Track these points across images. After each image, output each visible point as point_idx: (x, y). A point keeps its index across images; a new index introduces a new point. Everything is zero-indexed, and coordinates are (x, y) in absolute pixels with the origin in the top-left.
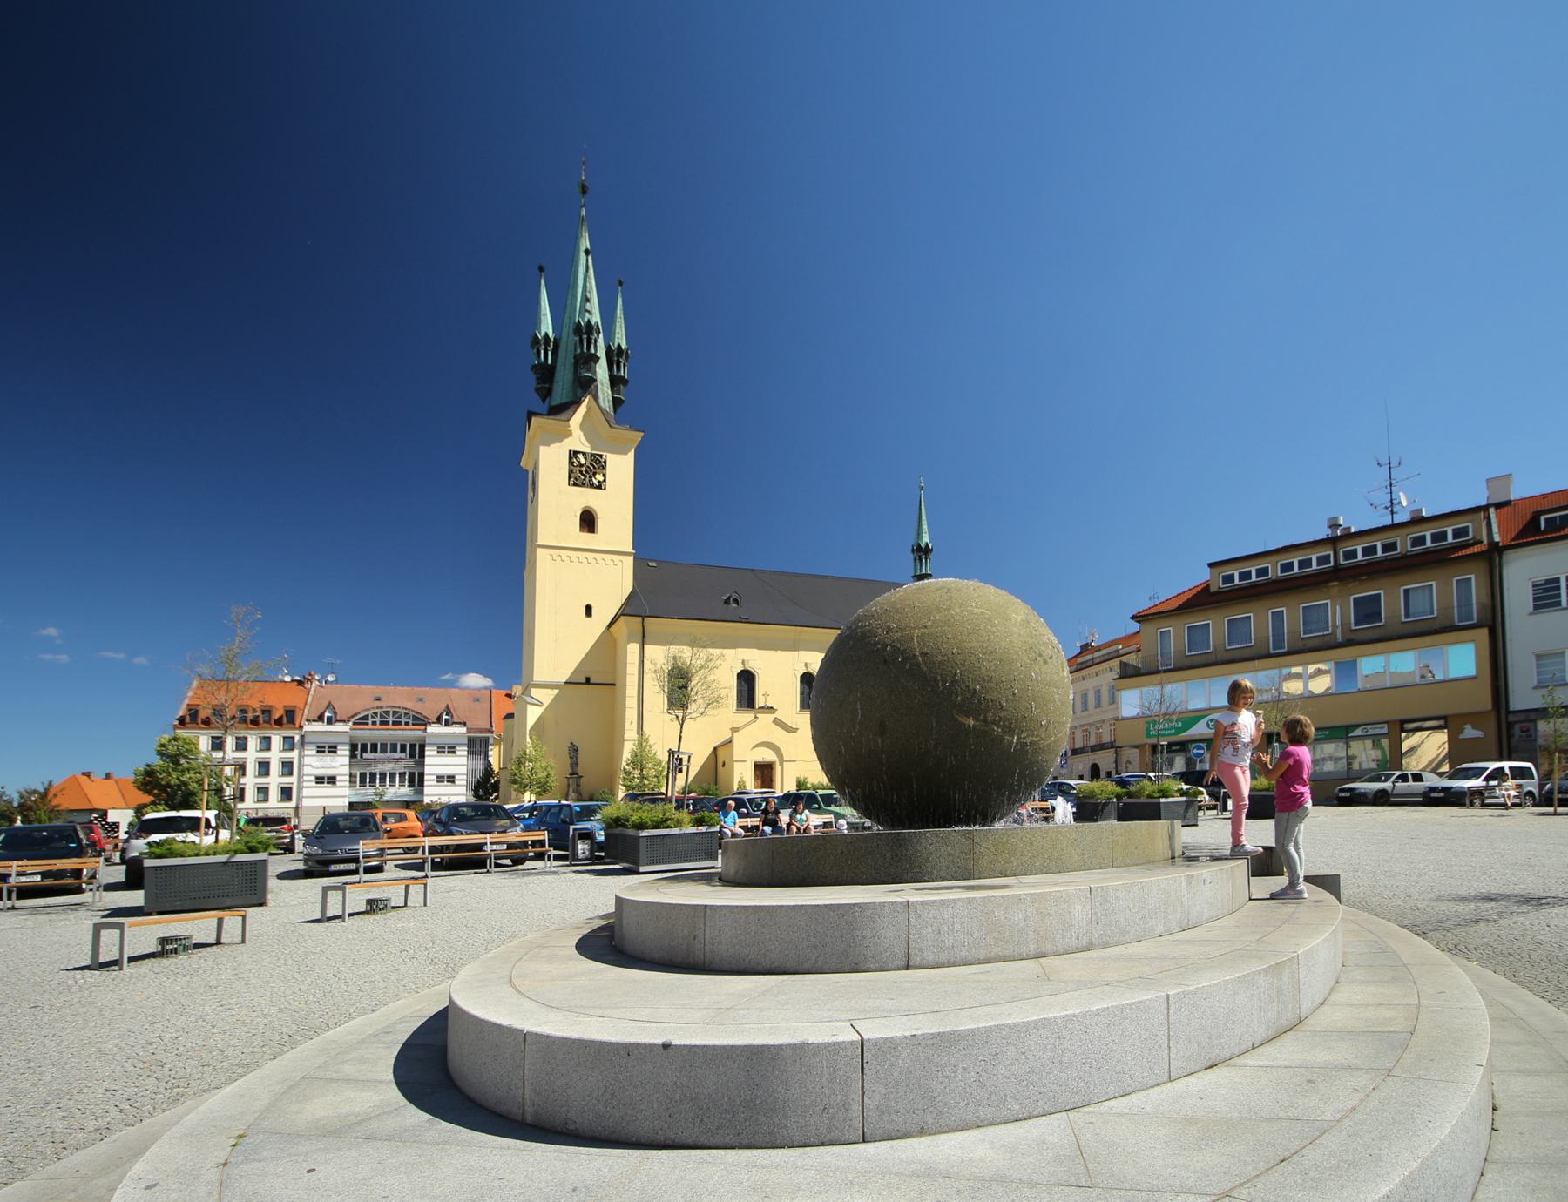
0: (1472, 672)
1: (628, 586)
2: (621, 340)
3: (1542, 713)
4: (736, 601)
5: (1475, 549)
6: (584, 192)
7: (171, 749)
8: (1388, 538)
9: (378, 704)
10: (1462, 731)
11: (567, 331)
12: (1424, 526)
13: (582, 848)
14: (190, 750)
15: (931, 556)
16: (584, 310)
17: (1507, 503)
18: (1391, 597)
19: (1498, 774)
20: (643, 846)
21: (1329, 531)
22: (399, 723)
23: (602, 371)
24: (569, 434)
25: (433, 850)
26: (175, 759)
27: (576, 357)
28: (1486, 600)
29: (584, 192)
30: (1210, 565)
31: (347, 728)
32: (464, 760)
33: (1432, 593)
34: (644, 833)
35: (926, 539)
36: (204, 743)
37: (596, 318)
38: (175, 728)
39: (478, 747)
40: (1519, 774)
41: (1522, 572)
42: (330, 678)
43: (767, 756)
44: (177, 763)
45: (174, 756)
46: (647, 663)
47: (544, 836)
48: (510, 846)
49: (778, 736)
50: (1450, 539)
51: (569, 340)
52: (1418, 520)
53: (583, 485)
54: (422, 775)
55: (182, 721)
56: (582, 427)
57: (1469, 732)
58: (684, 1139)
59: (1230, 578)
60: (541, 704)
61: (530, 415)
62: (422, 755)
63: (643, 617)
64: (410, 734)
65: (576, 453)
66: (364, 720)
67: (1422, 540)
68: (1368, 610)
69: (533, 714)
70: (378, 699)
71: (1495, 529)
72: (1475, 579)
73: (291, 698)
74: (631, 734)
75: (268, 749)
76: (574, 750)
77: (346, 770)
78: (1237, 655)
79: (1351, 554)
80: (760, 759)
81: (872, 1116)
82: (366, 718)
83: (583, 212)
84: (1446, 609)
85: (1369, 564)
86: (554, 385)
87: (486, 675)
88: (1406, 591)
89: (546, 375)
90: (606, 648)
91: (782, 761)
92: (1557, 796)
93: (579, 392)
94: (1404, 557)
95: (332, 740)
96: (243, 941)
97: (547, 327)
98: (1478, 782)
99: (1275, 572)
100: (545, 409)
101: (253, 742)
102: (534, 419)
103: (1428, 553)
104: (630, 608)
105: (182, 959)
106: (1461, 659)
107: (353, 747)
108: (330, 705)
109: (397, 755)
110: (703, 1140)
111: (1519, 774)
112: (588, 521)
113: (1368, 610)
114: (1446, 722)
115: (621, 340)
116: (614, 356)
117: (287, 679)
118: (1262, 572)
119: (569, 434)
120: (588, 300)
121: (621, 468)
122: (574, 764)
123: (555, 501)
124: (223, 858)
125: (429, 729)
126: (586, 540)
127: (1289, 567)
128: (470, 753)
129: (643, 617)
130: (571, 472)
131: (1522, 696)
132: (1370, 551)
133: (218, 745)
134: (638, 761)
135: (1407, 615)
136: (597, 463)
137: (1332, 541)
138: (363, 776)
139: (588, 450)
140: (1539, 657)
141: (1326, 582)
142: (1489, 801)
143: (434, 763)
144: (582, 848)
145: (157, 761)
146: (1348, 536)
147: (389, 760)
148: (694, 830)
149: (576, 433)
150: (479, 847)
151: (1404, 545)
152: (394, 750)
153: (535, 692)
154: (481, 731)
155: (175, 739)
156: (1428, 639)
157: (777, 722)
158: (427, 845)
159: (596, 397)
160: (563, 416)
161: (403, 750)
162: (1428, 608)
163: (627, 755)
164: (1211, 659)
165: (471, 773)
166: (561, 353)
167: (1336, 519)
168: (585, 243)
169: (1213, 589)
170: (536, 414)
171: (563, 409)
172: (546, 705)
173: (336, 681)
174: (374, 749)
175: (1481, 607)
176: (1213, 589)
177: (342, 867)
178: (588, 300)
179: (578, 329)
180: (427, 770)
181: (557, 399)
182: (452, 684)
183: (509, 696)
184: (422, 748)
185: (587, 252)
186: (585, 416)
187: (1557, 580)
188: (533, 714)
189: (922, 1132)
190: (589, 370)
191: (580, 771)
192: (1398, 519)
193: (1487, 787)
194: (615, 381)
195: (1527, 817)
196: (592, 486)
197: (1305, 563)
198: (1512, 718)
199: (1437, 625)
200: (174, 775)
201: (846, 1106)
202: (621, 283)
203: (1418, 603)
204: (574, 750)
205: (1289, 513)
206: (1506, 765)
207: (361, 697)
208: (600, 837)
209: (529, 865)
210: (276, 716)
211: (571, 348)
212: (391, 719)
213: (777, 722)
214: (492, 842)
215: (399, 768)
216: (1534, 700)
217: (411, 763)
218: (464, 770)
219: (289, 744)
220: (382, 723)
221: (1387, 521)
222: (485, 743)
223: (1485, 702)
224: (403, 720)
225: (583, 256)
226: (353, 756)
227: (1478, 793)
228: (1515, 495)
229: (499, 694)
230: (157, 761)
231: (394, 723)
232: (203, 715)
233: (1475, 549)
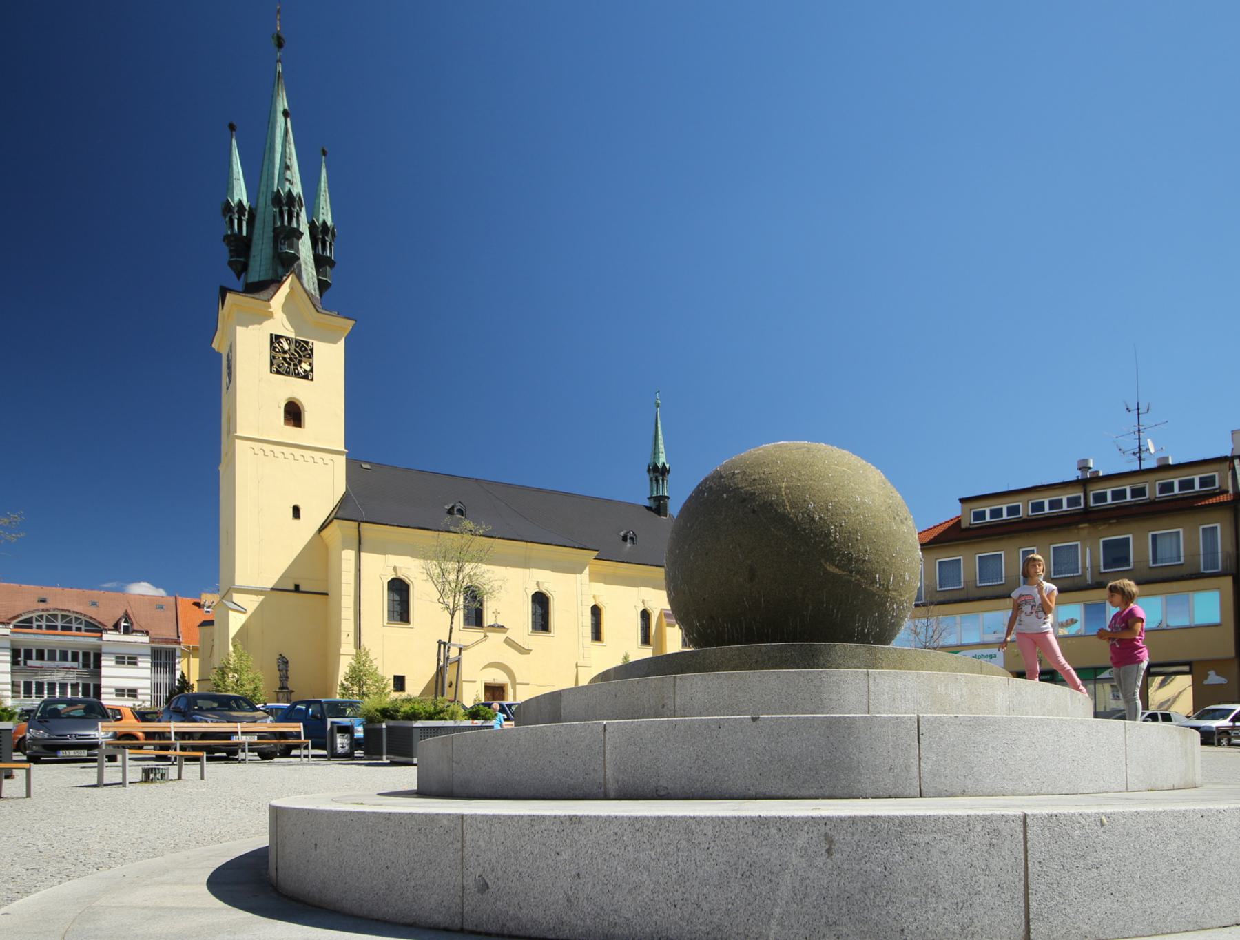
0: (1216, 619)
1: (341, 488)
2: (326, 215)
4: (460, 512)
5: (1222, 498)
6: (280, 44)
8: (1138, 482)
9: (42, 605)
10: (1206, 677)
11: (264, 201)
12: (1172, 473)
13: (341, 742)
15: (669, 477)
18: (1139, 541)
20: (416, 735)
21: (1079, 473)
22: (70, 629)
23: (305, 248)
24: (270, 316)
27: (275, 230)
29: (280, 44)
30: (962, 500)
32: (148, 673)
35: (662, 459)
37: (297, 189)
39: (163, 658)
43: (499, 677)
47: (299, 727)
48: (261, 736)
50: (1197, 487)
51: (266, 212)
52: (1164, 467)
53: (287, 373)
56: (285, 308)
57: (1213, 678)
59: (980, 515)
60: (244, 611)
61: (224, 292)
62: (98, 665)
63: (359, 522)
64: (86, 640)
65: (278, 337)
66: (27, 624)
67: (1169, 487)
68: (1117, 555)
69: (236, 622)
70: (43, 601)
74: (347, 647)
76: (283, 662)
78: (989, 592)
79: (1101, 497)
80: (490, 680)
81: (926, 778)
82: (29, 620)
83: (280, 68)
86: (252, 258)
87: (157, 586)
88: (1154, 537)
89: (240, 248)
90: (317, 553)
91: (514, 684)
93: (280, 270)
96: (28, 795)
97: (240, 193)
98: (1225, 723)
99: (1026, 511)
100: (240, 285)
102: (229, 296)
104: (344, 511)
107: (15, 653)
109: (69, 664)
110: (791, 792)
112: (294, 414)
113: (1117, 555)
114: (1194, 667)
115: (326, 215)
116: (319, 234)
118: (1013, 510)
119: (270, 316)
120: (288, 168)
121: (330, 358)
122: (284, 678)
123: (255, 392)
125: (106, 637)
127: (1039, 506)
129: (359, 522)
130: (273, 358)
132: (1119, 495)
134: (357, 676)
136: (303, 351)
137: (1083, 483)
138: (28, 685)
139: (292, 335)
141: (1078, 523)
142: (1235, 741)
143: (113, 676)
144: (341, 742)
146: (1097, 479)
148: (469, 723)
149: (279, 314)
150: (228, 735)
151: (1153, 490)
152: (64, 657)
153: (237, 597)
154: (167, 641)
156: (1175, 585)
157: (508, 641)
158: (173, 730)
159: (299, 277)
161: (75, 657)
162: (1175, 555)
163: (344, 669)
164: (962, 595)
165: (155, 687)
167: (1086, 461)
168: (282, 104)
169: (964, 525)
170: (231, 291)
171: (263, 287)
172: (250, 612)
174: (40, 655)
176: (964, 525)
177: (71, 753)
178: (288, 168)
179: (277, 199)
180: (104, 682)
181: (254, 276)
183: (198, 605)
184: (98, 657)
185: (286, 114)
186: (289, 297)
188: (236, 622)
189: (964, 794)
190: (291, 247)
191: (290, 684)
192: (1145, 466)
193: (1233, 728)
194: (321, 262)
196: (297, 375)
199: (1184, 571)
201: (907, 768)
202: (324, 153)
203: (1165, 548)
204: (283, 662)
205: (1041, 452)
208: (359, 733)
209: (276, 760)
211: (270, 220)
212: (59, 624)
213: (508, 641)
215: (71, 678)
217: (85, 674)
218: (148, 683)
220: (49, 627)
222: (171, 655)
224: (74, 626)
225: (280, 119)
226: (15, 662)
227: (1224, 732)
229: (185, 602)
231: (63, 628)
233: (1222, 498)
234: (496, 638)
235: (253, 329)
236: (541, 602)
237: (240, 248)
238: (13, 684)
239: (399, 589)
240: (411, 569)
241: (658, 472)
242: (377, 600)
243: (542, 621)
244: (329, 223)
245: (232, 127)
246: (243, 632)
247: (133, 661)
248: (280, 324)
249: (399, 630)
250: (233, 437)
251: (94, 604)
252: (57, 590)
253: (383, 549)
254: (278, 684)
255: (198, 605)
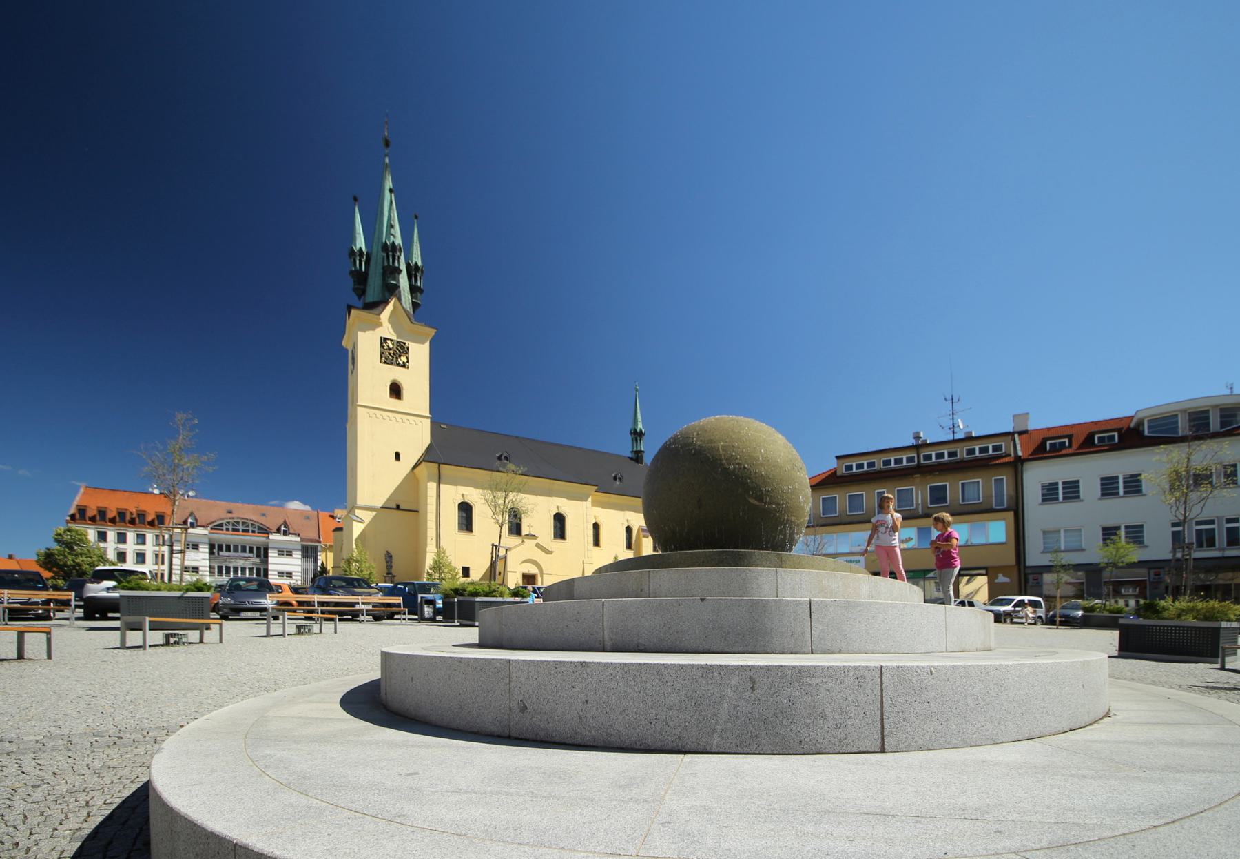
0: (1003, 539)
1: (427, 441)
2: (417, 259)
3: (1048, 569)
4: (506, 458)
5: (1007, 460)
6: (387, 144)
7: (67, 538)
8: (952, 448)
11: (376, 249)
14: (83, 539)
15: (644, 438)
16: (389, 234)
17: (1025, 432)
18: (953, 486)
19: (1021, 604)
20: (477, 607)
23: (403, 280)
24: (380, 325)
25: (321, 604)
26: (69, 546)
27: (384, 268)
28: (1013, 493)
29: (387, 144)
30: (838, 457)
31: (205, 532)
32: (299, 562)
33: (980, 486)
34: (478, 599)
35: (640, 426)
36: (92, 534)
38: (67, 522)
39: (309, 552)
40: (1035, 604)
41: (1036, 476)
42: (191, 493)
43: (532, 569)
44: (71, 549)
45: (69, 544)
46: (443, 498)
47: (400, 600)
48: (375, 605)
49: (539, 556)
50: (991, 452)
51: (378, 255)
52: (969, 438)
54: (266, 571)
55: (73, 517)
56: (390, 320)
57: (1001, 579)
58: (715, 649)
59: (850, 468)
61: (349, 308)
62: (266, 556)
64: (259, 539)
65: (385, 339)
66: (219, 527)
68: (938, 495)
69: (357, 529)
70: (230, 512)
71: (1019, 448)
72: (1006, 478)
73: (163, 507)
74: (431, 548)
75: (144, 543)
76: (389, 557)
77: (207, 563)
79: (928, 457)
80: (526, 571)
82: (221, 525)
83: (387, 160)
84: (987, 497)
85: (940, 464)
86: (368, 287)
87: (305, 503)
89: (361, 279)
90: (411, 484)
92: (1058, 619)
93: (387, 294)
94: (962, 461)
95: (289, 547)
97: (361, 243)
98: (1009, 608)
99: (879, 465)
100: (360, 305)
101: (131, 536)
102: (353, 311)
103: (977, 460)
104: (430, 456)
105: (182, 647)
106: (997, 531)
107: (212, 547)
108: (191, 514)
109: (247, 554)
110: (726, 649)
111: (1035, 604)
112: (396, 390)
113: (938, 495)
114: (988, 571)
115: (417, 259)
116: (413, 271)
117: (156, 492)
118: (871, 465)
119: (380, 325)
120: (392, 226)
121: (420, 354)
122: (389, 567)
123: (370, 376)
124: (178, 594)
125: (271, 537)
126: (394, 404)
128: (303, 556)
130: (382, 353)
131: (1035, 557)
133: (102, 536)
134: (437, 566)
135: (963, 500)
136: (402, 349)
137: (916, 448)
138: (220, 568)
139: (395, 338)
140: (1044, 532)
141: (912, 474)
143: (276, 563)
144: (428, 610)
145: (55, 547)
147: (241, 558)
148: (512, 599)
149: (386, 324)
150: (352, 604)
151: (962, 454)
152: (244, 550)
153: (358, 512)
154: (312, 541)
155: (69, 530)
156: (976, 516)
157: (538, 545)
159: (399, 299)
160: (376, 311)
161: (251, 550)
165: (304, 571)
166: (372, 263)
168: (389, 184)
169: (839, 473)
171: (375, 306)
172: (367, 522)
173: (196, 496)
175: (1009, 498)
176: (839, 473)
177: (249, 614)
179: (385, 247)
180: (270, 567)
181: (370, 298)
182: (281, 506)
183: (332, 517)
184: (266, 550)
185: (391, 191)
187: (1057, 484)
188: (357, 529)
190: (394, 279)
191: (394, 571)
192: (957, 437)
194: (414, 290)
195: (1040, 629)
196: (398, 365)
197: (898, 461)
198: (1028, 571)
200: (70, 557)
201: (803, 634)
203: (970, 491)
204: (389, 557)
205: (888, 429)
206: (1026, 598)
207: (217, 509)
208: (440, 604)
210: (149, 518)
211: (380, 261)
212: (241, 528)
213: (538, 545)
214: (362, 601)
216: (1044, 560)
217: (258, 561)
218: (299, 569)
219: (159, 541)
220: (234, 530)
221: (950, 437)
223: (1011, 560)
225: (387, 194)
226: (211, 553)
227: (1008, 614)
228: (1031, 426)
229: (324, 515)
230: (55, 547)
232: (90, 513)
233: (1007, 460)
234: (532, 542)
235: (369, 333)
236: (560, 519)
237: (361, 279)
238: (211, 567)
239: (466, 510)
240: (473, 495)
241: (637, 435)
242: (451, 516)
243: (560, 533)
244: (420, 264)
245: (355, 199)
246: (362, 535)
247: (289, 554)
248: (387, 330)
249: (465, 536)
250: (355, 406)
251: (264, 515)
252: (240, 505)
253: (455, 483)
254: (385, 571)
255: (332, 517)
